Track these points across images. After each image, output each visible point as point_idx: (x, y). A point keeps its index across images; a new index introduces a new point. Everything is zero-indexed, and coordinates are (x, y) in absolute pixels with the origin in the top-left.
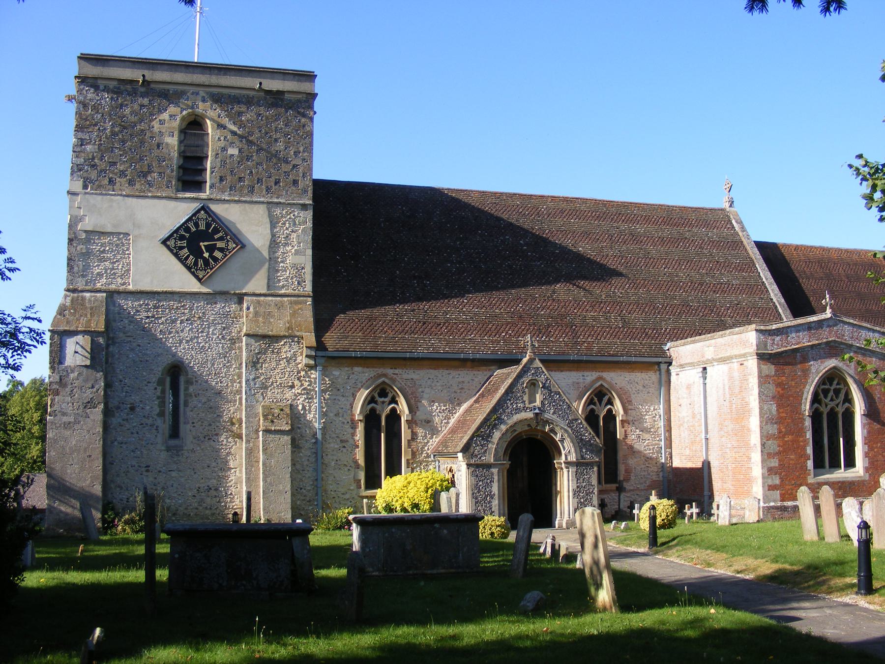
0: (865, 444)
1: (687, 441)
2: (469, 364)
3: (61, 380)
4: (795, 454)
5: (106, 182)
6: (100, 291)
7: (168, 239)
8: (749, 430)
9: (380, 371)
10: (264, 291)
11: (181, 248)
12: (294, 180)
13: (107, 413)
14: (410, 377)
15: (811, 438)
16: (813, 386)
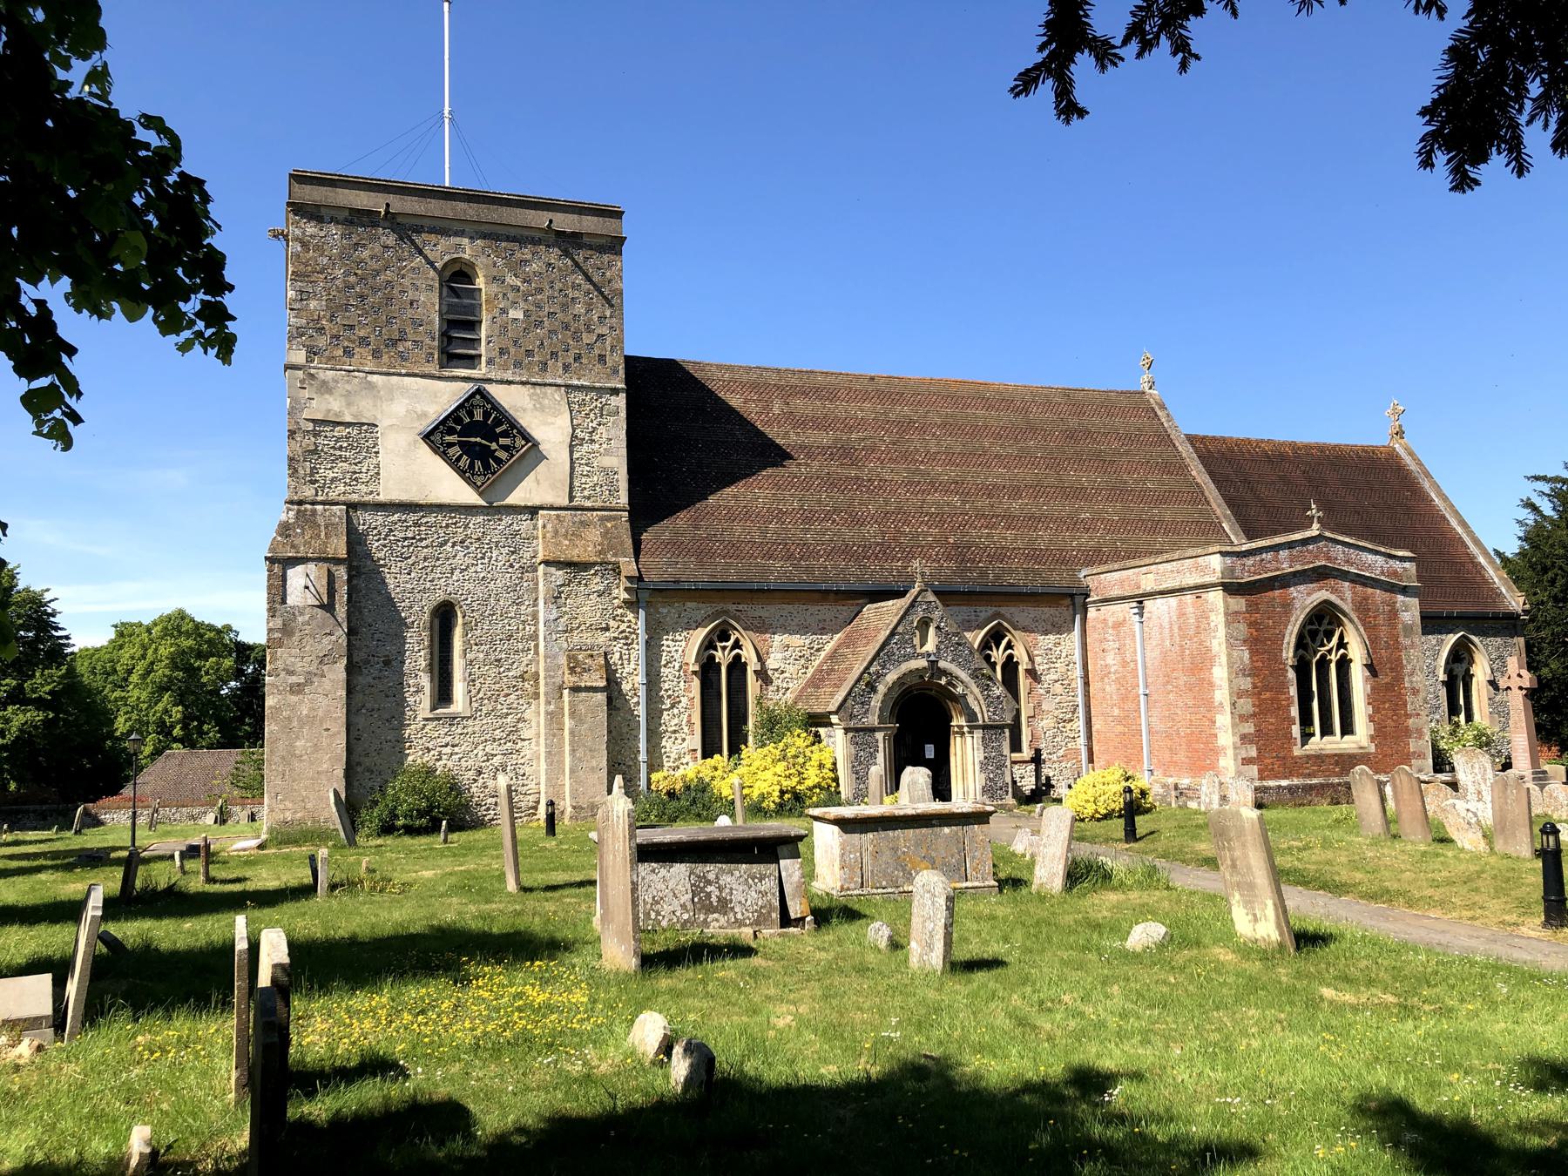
0: (1369, 704)
1: (1115, 697)
2: (832, 596)
3: (284, 625)
4: (1276, 717)
5: (340, 352)
6: (337, 504)
7: (432, 432)
8: (1211, 685)
9: (719, 607)
10: (566, 502)
11: (450, 445)
12: (599, 355)
13: (351, 669)
14: (757, 614)
15: (1296, 696)
16: (1298, 626)
